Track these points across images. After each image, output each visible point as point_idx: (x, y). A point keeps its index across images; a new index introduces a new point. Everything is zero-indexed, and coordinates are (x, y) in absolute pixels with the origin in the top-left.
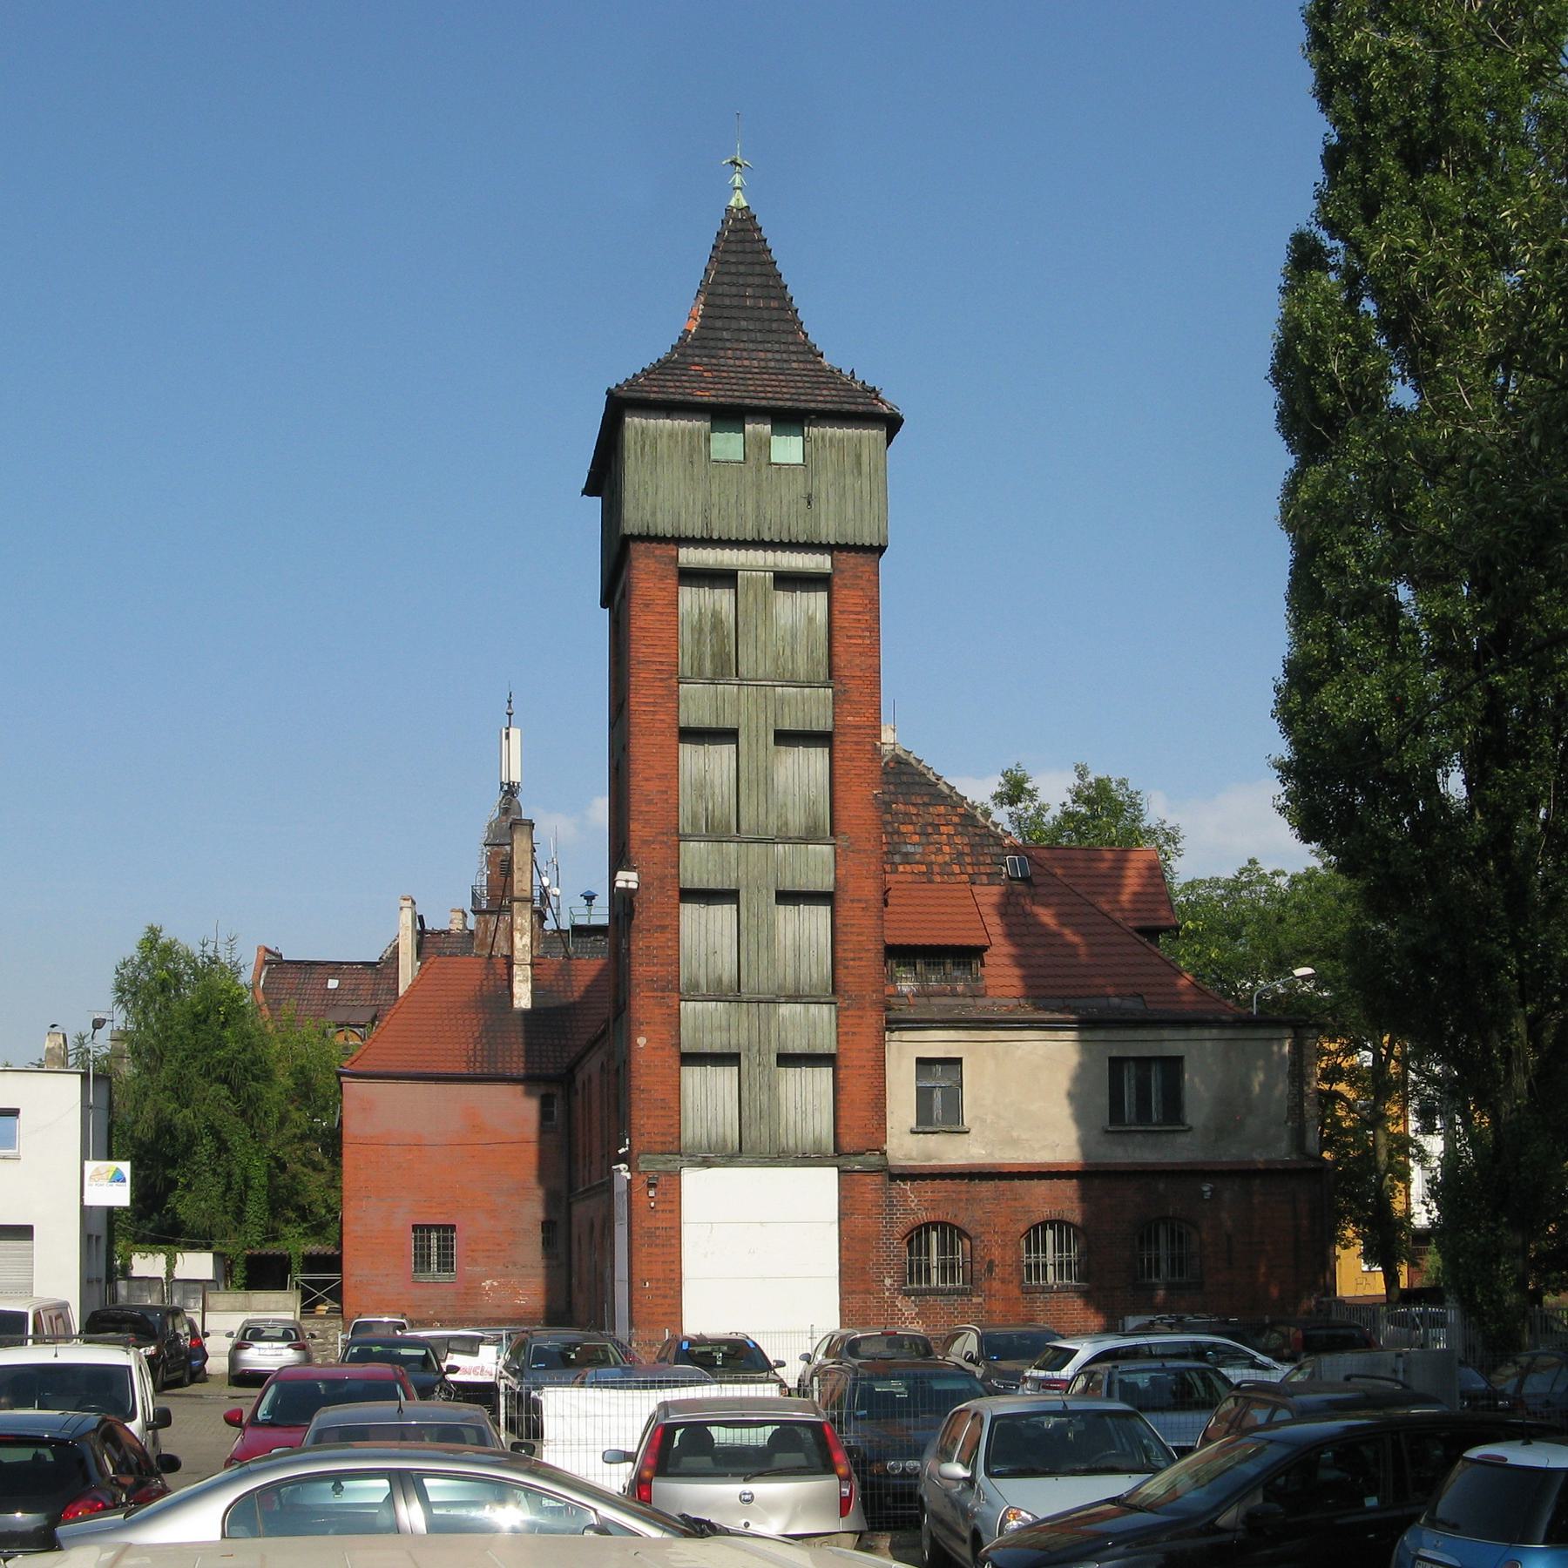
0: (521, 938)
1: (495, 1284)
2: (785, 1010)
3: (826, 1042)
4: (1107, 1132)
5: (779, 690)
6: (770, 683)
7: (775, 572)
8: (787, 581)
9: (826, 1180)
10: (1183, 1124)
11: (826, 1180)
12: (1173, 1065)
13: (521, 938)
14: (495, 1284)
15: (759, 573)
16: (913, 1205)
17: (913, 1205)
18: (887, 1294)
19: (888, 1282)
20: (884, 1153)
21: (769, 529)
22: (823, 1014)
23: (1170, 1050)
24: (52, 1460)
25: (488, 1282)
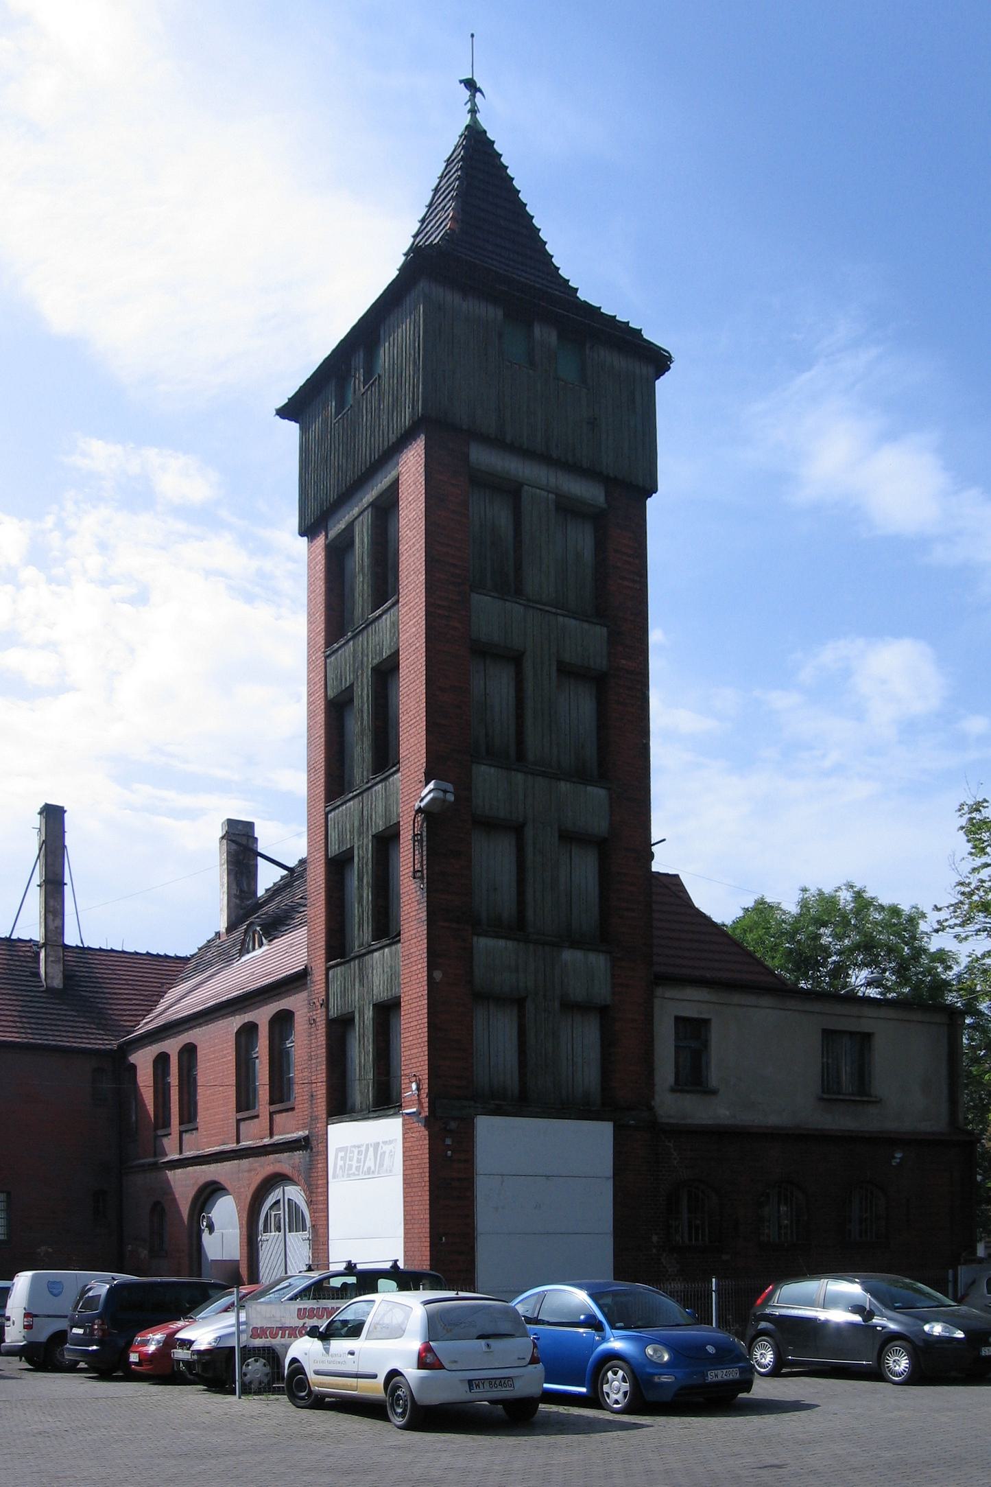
0: (53, 920)
1: (50, 1250)
2: (568, 955)
3: (602, 991)
4: (821, 1099)
5: (561, 619)
6: (554, 610)
7: (557, 495)
8: (567, 508)
9: (603, 1133)
10: (871, 1096)
11: (603, 1133)
12: (865, 1039)
13: (53, 920)
14: (50, 1250)
15: (543, 492)
16: (675, 1162)
17: (675, 1162)
18: (654, 1251)
19: (655, 1239)
20: (651, 1109)
21: (557, 446)
22: (599, 962)
23: (865, 1026)
24: (983, 1353)
25: (43, 1248)
